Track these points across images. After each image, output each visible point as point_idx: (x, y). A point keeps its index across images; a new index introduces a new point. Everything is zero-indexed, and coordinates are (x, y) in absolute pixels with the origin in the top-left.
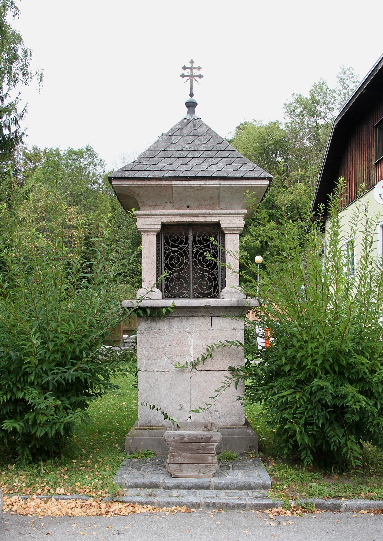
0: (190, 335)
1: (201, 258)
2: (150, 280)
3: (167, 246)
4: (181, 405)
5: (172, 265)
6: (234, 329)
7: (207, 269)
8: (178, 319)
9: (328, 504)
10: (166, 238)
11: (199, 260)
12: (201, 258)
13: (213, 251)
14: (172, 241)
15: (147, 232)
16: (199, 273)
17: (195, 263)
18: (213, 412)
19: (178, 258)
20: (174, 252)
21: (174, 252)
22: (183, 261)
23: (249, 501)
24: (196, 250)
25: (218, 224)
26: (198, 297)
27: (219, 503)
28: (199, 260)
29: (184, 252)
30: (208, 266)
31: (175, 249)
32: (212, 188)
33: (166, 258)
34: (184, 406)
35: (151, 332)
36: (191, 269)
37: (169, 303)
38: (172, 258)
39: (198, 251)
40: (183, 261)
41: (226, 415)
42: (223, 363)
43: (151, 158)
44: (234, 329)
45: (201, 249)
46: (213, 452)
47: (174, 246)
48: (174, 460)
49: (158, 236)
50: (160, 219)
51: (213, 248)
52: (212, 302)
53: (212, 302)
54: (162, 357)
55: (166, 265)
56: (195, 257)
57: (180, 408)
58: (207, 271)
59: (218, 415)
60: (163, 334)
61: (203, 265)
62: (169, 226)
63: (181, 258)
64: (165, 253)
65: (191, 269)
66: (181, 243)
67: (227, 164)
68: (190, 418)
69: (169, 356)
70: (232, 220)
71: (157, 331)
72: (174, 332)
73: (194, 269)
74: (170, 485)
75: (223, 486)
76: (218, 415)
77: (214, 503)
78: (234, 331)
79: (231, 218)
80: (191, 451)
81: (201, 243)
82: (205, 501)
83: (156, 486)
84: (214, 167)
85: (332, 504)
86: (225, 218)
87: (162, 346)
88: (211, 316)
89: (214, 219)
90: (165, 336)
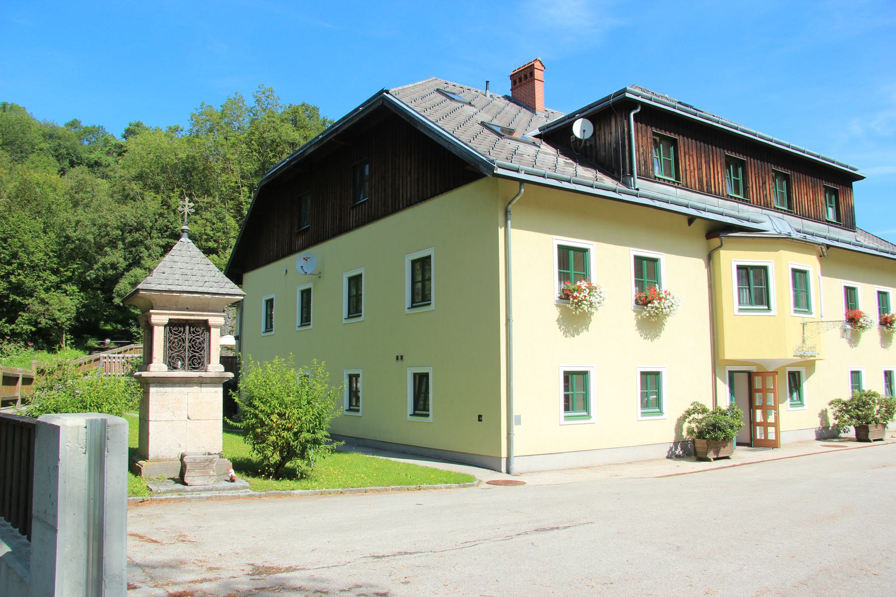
15: (158, 325)
25: (206, 321)
32: (194, 297)
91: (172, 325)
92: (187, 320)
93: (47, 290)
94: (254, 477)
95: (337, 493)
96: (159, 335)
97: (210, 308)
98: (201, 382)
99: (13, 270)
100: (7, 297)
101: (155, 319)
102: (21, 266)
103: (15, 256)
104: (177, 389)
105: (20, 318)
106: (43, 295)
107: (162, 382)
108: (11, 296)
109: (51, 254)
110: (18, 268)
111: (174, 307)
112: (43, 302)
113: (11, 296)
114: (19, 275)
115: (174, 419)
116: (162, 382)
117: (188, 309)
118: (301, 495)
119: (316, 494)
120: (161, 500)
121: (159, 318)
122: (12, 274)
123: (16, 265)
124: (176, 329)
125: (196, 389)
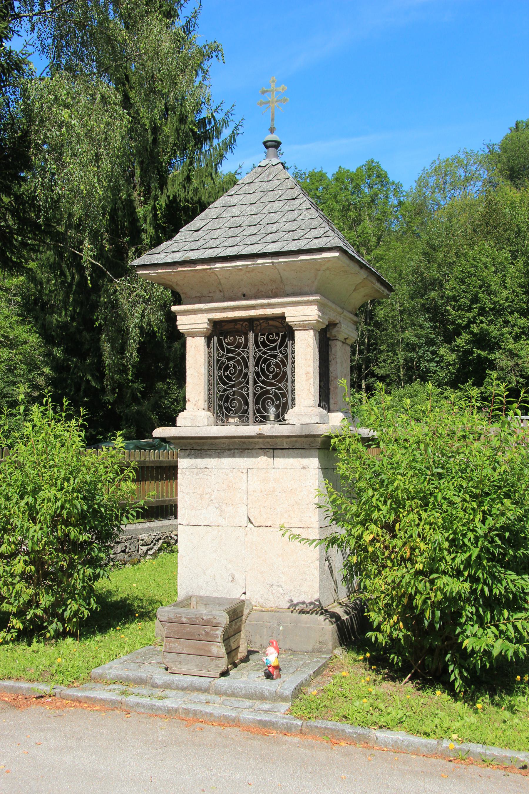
0: (244, 476)
1: (264, 367)
2: (196, 399)
3: (221, 352)
4: (233, 575)
5: (228, 377)
6: (304, 467)
7: (273, 381)
8: (229, 452)
9: (350, 733)
10: (220, 341)
11: (262, 370)
12: (264, 367)
13: (281, 355)
14: (228, 344)
15: (194, 335)
16: (262, 388)
17: (257, 374)
18: (275, 587)
19: (235, 367)
20: (229, 359)
21: (229, 359)
22: (241, 371)
23: (247, 715)
24: (258, 356)
25: (282, 317)
26: (261, 421)
27: (201, 711)
28: (262, 370)
29: (243, 358)
30: (274, 377)
31: (230, 355)
32: (240, 269)
33: (220, 369)
34: (237, 576)
35: (195, 471)
36: (251, 382)
37: (234, 429)
38: (227, 368)
39: (260, 357)
40: (241, 371)
41: (293, 592)
42: (289, 516)
43: (196, 231)
44: (304, 467)
45: (264, 353)
46: (218, 640)
47: (229, 351)
48: (170, 648)
49: (209, 340)
50: (205, 315)
51: (281, 352)
52: (270, 429)
53: (270, 429)
54: (209, 505)
55: (220, 377)
56: (257, 365)
57: (231, 579)
58: (272, 385)
59: (282, 592)
60: (210, 474)
61: (267, 376)
62: (223, 324)
63: (239, 368)
64: (218, 361)
65: (251, 382)
66: (238, 347)
67: (289, 232)
68: (245, 593)
69: (217, 505)
70: (303, 312)
71: (203, 470)
72: (224, 470)
73: (255, 382)
74: (159, 682)
75: (226, 690)
76: (282, 592)
77: (194, 710)
78: (303, 471)
79: (300, 308)
80: (191, 637)
81: (264, 345)
82: (185, 706)
83: (140, 682)
84: (269, 238)
85: (356, 733)
86: (291, 308)
87: (209, 490)
88: (274, 449)
89: (277, 311)
90: (213, 477)
91: (219, 330)
92: (251, 320)
93: (517, 338)
94: (303, 681)
95: (506, 766)
96: (197, 357)
97: (289, 289)
98: (273, 447)
99: (474, 318)
100: (472, 353)
101: (184, 323)
102: (482, 311)
103: (475, 300)
104: (227, 462)
105: (488, 379)
106: (511, 345)
107: (200, 447)
108: (475, 350)
109: (519, 290)
110: (479, 315)
111: (218, 295)
112: (512, 354)
113: (475, 350)
114: (482, 322)
115: (223, 523)
116: (200, 447)
117: (245, 297)
118: (398, 749)
119: (443, 755)
120: (78, 700)
121: (192, 320)
122: (474, 322)
123: (476, 310)
124: (229, 339)
125: (263, 461)
